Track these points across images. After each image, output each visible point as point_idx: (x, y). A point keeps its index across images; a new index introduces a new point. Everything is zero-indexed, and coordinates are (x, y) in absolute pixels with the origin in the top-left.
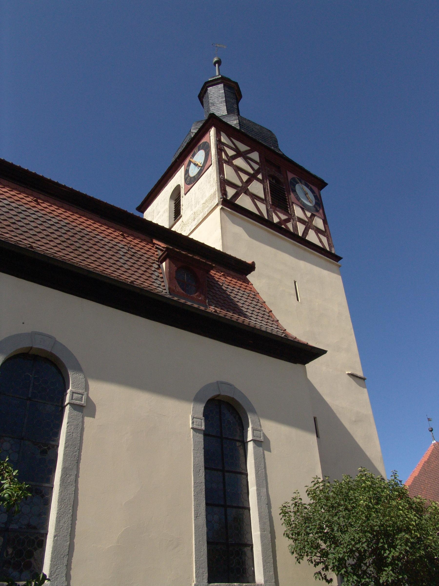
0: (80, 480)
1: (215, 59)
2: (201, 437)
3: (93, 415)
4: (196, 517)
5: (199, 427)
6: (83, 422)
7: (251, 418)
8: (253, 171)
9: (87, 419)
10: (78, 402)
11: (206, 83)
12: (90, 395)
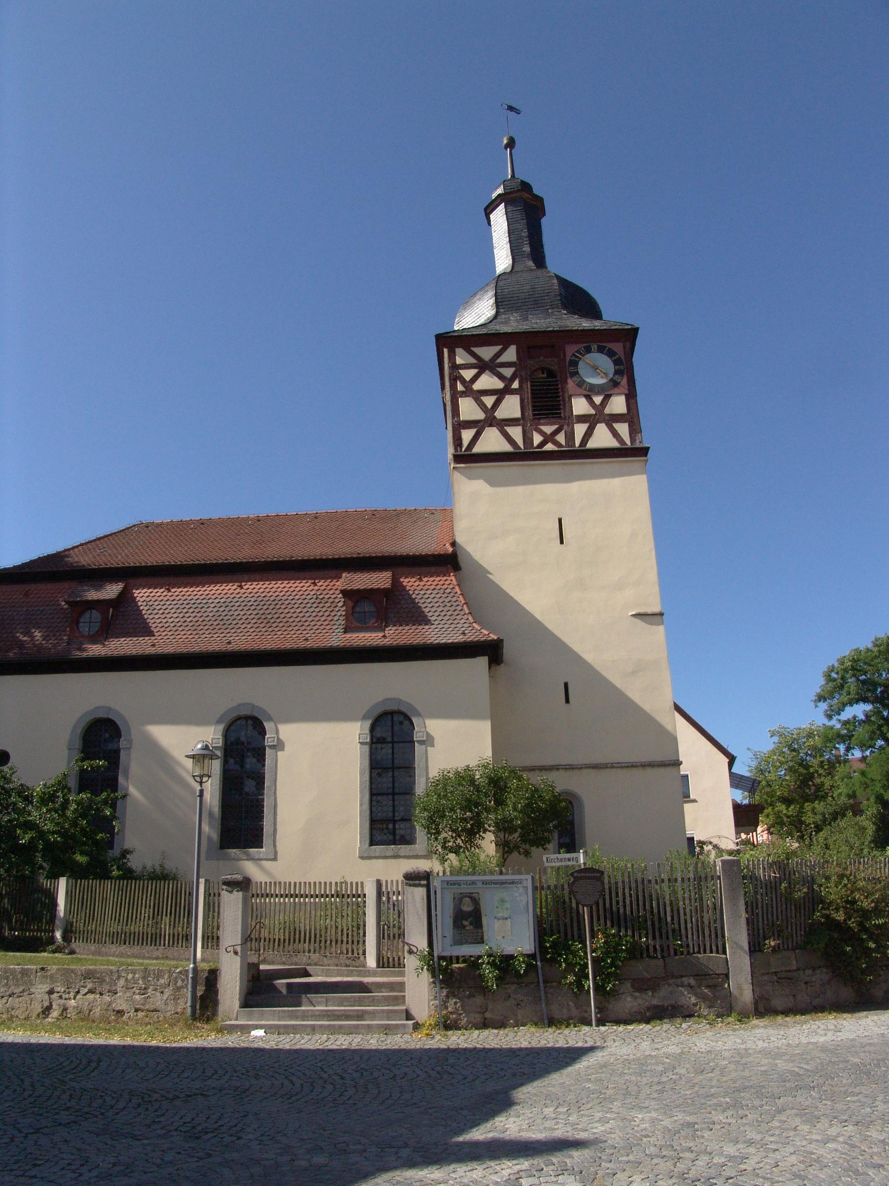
0: (277, 792)
1: (505, 141)
2: (367, 749)
3: (433, 746)
4: (361, 805)
5: (365, 741)
6: (277, 756)
7: (268, 726)
8: (503, 381)
9: (429, 748)
10: (272, 744)
11: (486, 209)
12: (280, 737)
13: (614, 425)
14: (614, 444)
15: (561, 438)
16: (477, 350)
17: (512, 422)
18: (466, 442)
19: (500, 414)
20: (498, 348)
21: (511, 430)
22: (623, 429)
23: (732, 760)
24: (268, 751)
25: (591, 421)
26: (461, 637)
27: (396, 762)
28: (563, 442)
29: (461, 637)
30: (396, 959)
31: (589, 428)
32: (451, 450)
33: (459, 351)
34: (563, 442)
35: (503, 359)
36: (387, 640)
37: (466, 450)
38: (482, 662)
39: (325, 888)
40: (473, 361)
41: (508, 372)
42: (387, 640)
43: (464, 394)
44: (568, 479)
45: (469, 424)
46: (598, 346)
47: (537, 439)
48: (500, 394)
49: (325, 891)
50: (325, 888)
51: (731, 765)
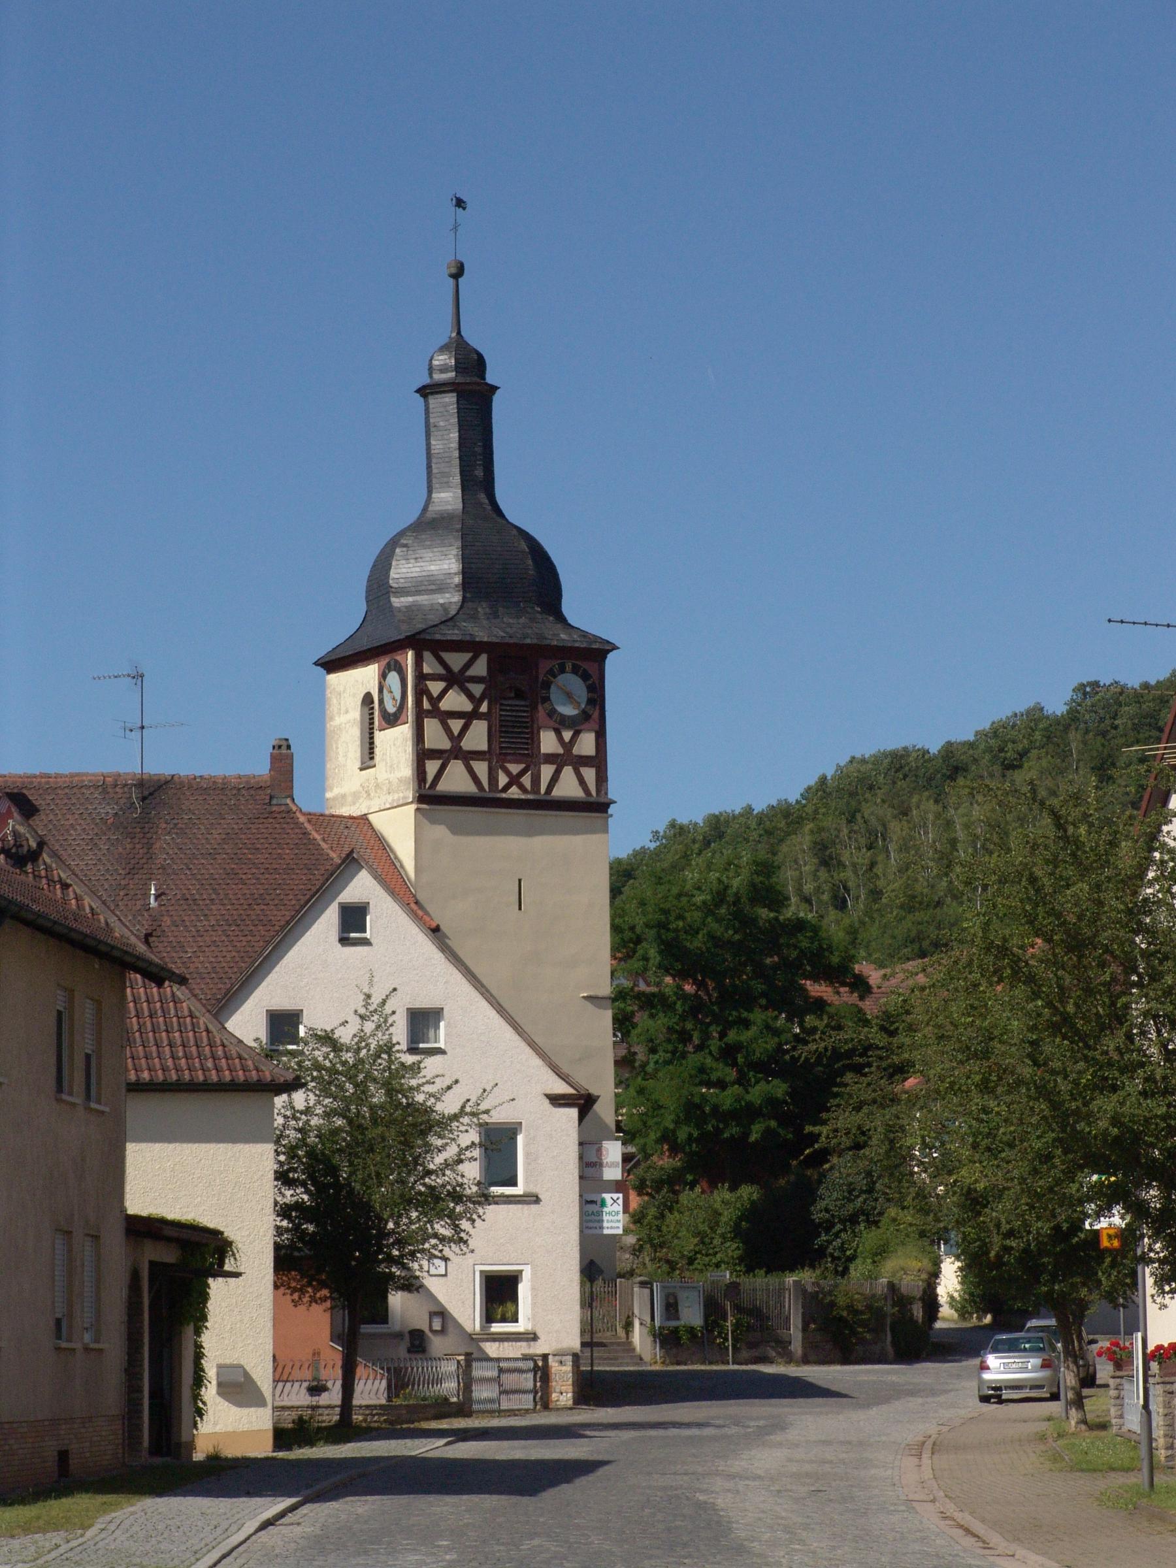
15: (526, 780)
17: (477, 755)
18: (430, 777)
19: (467, 744)
22: (589, 774)
31: (466, 671)
37: (429, 788)
44: (530, 832)
48: (469, 718)
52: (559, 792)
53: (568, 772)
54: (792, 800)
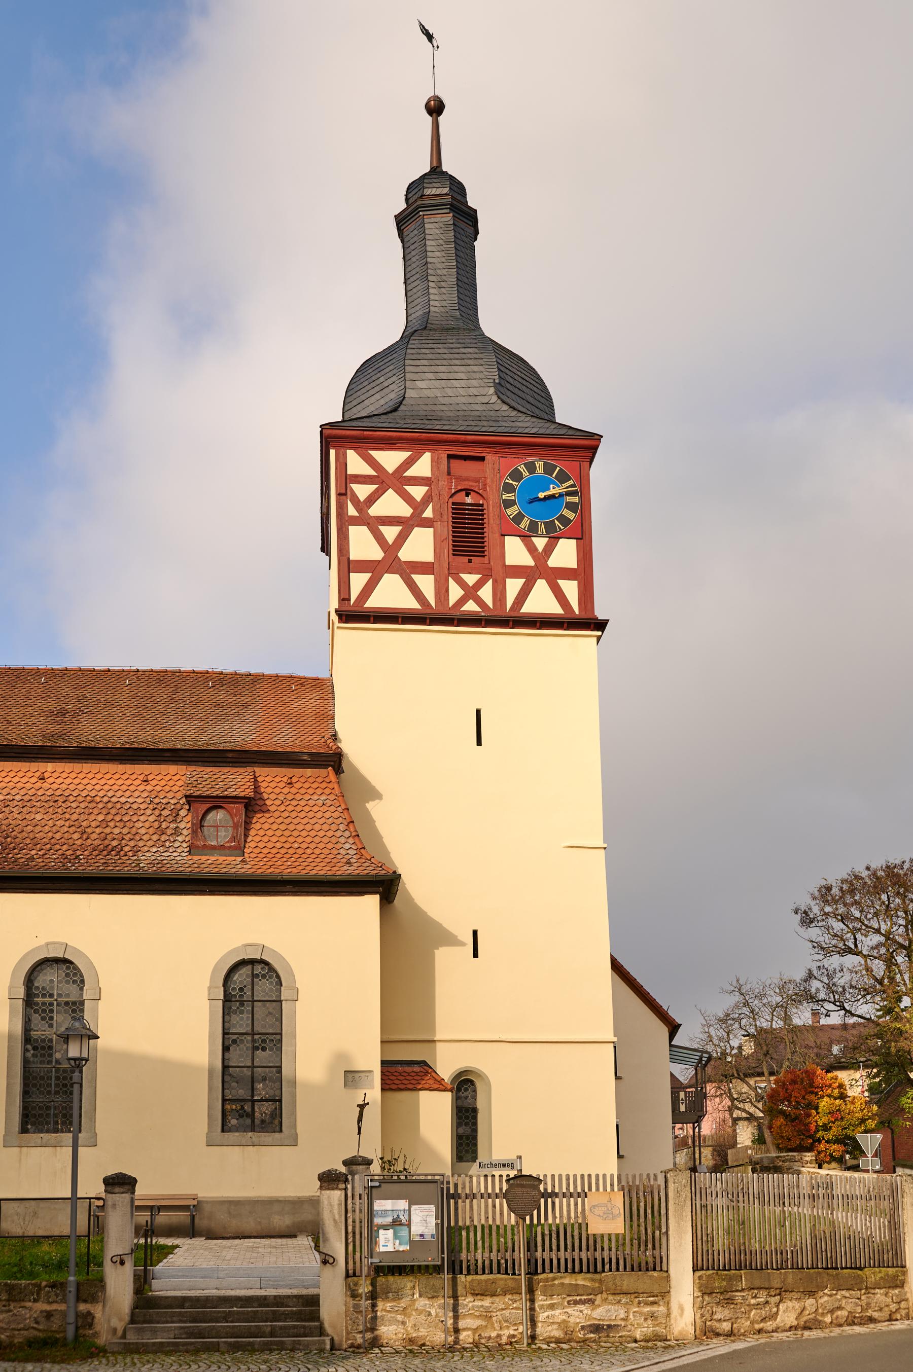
13: (560, 582)
14: (555, 609)
15: (486, 593)
16: (377, 455)
17: (424, 568)
19: (406, 554)
20: (405, 455)
21: (419, 579)
22: (570, 588)
23: (673, 1028)
24: (87, 1005)
25: (530, 575)
26: (346, 868)
27: (255, 1029)
28: (489, 601)
29: (346, 868)
30: (487, 1263)
31: (536, 549)
32: (334, 604)
33: (352, 455)
34: (489, 601)
35: (415, 471)
36: (248, 866)
38: (372, 902)
39: (568, 1185)
40: (370, 472)
41: (418, 492)
42: (248, 866)
43: (355, 521)
45: (363, 566)
46: (545, 464)
47: (455, 592)
48: (407, 525)
49: (568, 1188)
50: (568, 1185)
51: (672, 1036)
52: (530, 607)
53: (541, 585)
54: (337, 416)
